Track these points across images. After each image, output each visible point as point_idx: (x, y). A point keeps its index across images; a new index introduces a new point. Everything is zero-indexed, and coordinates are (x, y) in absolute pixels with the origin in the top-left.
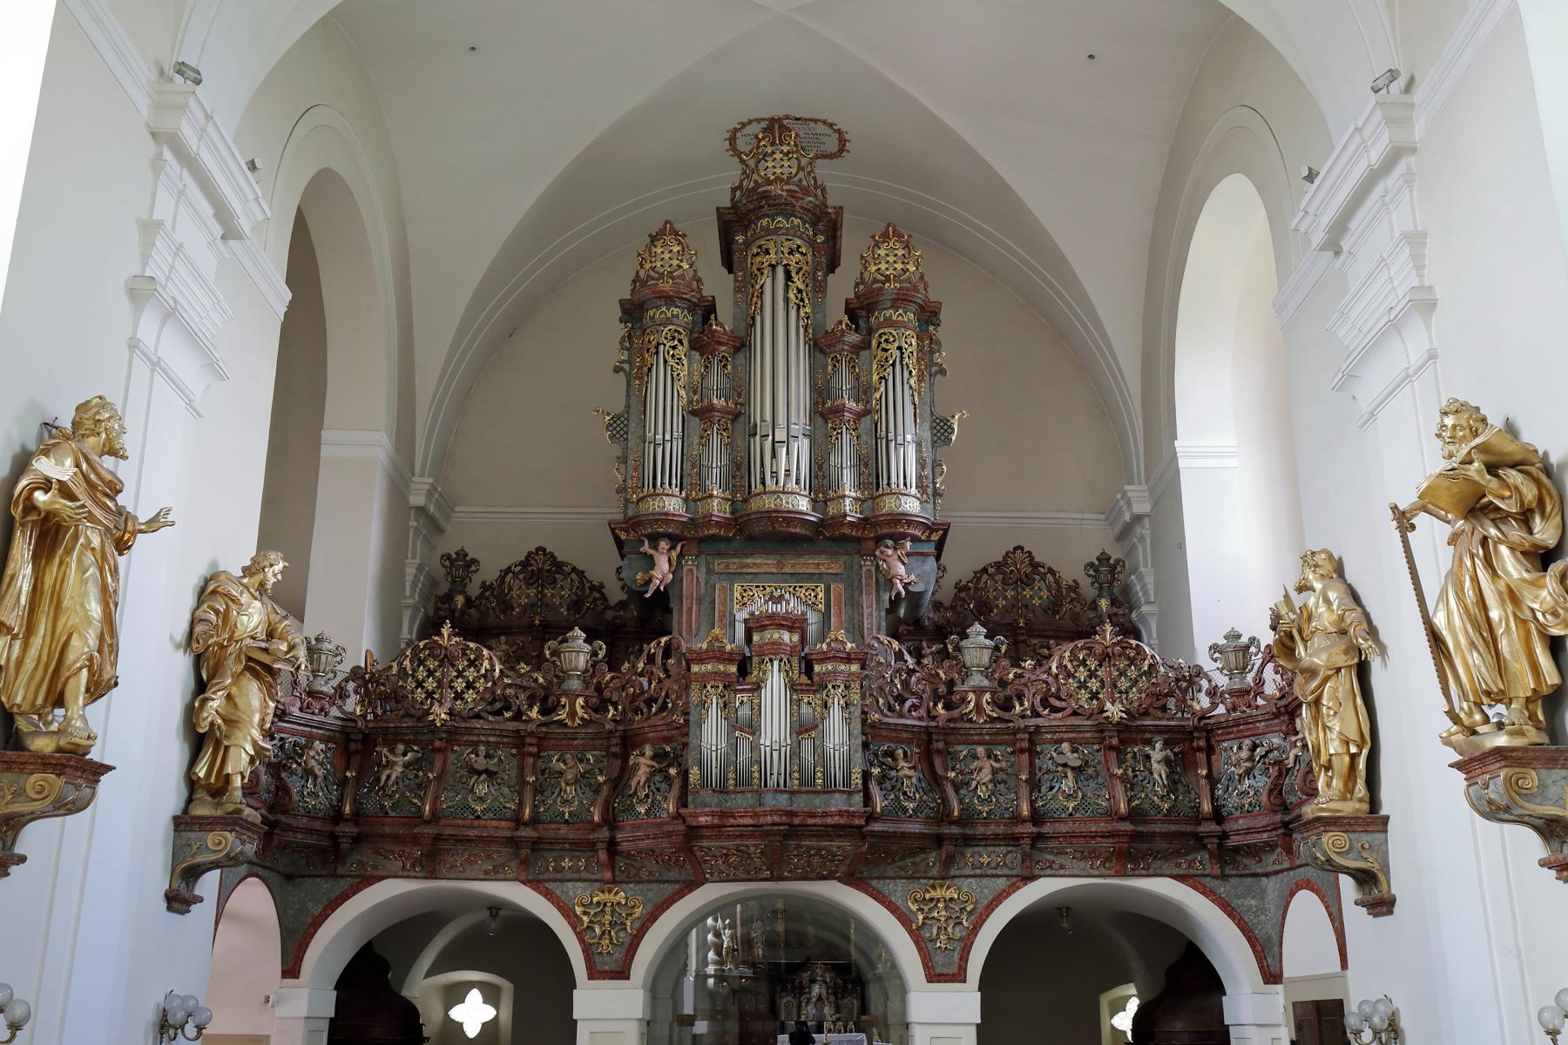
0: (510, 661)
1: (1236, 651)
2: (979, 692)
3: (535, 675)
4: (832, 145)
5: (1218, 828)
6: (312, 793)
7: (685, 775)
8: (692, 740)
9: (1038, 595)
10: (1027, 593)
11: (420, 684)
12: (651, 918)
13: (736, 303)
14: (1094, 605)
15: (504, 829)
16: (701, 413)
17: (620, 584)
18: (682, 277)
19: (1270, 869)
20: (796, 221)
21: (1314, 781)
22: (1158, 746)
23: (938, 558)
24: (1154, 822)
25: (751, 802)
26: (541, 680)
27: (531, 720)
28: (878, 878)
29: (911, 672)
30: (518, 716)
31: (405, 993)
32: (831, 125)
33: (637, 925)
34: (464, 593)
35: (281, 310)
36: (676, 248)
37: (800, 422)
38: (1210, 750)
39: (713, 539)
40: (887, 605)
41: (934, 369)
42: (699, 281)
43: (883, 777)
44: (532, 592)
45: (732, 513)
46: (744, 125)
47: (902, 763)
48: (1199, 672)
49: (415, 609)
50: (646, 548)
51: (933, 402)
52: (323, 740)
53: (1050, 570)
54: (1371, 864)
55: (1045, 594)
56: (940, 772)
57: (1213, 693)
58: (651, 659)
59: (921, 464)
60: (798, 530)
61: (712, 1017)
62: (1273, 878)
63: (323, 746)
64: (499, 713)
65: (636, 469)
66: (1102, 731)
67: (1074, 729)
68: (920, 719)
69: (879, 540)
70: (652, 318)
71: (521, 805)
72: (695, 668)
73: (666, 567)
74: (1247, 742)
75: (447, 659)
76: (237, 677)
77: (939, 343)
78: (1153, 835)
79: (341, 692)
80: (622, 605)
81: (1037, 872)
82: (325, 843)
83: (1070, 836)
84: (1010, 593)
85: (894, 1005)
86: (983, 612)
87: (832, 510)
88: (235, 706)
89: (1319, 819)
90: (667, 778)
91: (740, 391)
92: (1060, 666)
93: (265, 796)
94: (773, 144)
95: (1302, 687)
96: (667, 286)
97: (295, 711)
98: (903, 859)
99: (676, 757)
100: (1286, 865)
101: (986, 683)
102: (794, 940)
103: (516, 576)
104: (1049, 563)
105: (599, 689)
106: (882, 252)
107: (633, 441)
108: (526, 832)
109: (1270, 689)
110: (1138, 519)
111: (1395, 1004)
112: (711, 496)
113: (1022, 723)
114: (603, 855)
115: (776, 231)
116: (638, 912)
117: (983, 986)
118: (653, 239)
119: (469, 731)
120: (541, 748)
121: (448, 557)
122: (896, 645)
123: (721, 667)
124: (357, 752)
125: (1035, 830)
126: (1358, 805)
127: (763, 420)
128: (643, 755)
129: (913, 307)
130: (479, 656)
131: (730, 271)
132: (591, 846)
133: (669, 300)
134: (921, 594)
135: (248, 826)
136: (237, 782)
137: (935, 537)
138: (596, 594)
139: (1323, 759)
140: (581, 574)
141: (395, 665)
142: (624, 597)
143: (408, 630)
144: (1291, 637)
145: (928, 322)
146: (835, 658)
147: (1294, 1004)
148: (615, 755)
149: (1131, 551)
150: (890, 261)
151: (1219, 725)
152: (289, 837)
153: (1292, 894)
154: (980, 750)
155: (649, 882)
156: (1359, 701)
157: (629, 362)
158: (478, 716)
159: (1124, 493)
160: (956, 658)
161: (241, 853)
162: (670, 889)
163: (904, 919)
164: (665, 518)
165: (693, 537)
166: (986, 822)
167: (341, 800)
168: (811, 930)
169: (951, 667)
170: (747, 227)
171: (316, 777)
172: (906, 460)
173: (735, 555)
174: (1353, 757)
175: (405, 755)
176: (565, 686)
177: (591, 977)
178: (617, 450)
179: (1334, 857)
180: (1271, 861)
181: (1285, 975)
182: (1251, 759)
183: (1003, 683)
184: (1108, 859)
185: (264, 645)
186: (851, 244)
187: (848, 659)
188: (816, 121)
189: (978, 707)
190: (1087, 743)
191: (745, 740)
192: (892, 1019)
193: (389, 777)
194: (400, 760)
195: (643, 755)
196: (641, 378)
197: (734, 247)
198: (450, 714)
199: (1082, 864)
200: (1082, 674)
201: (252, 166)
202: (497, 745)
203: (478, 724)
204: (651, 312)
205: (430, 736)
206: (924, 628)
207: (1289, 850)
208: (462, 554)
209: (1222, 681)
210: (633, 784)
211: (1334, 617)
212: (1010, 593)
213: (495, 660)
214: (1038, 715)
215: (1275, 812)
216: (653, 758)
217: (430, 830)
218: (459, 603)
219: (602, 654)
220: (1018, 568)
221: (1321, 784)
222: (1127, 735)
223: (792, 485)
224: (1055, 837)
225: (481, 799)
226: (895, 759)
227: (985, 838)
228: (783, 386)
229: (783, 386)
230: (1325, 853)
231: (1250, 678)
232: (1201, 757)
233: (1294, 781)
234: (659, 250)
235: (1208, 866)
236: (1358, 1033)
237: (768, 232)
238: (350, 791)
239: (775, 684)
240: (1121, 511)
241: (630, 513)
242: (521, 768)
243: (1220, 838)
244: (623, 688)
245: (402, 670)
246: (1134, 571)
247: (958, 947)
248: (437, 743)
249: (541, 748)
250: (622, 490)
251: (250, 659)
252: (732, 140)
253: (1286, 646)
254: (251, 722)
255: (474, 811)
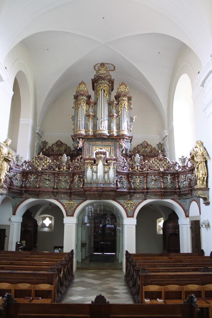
0: (53, 161)
1: (183, 160)
2: (138, 166)
3: (57, 162)
4: (113, 69)
5: (179, 191)
6: (17, 183)
7: (84, 181)
8: (85, 174)
9: (148, 150)
10: (146, 149)
11: (36, 164)
12: (78, 206)
13: (95, 96)
14: (158, 152)
15: (51, 190)
16: (88, 116)
17: (73, 147)
18: (85, 91)
19: (188, 198)
20: (106, 81)
21: (197, 181)
22: (169, 176)
23: (131, 143)
24: (168, 189)
25: (96, 185)
26: (58, 163)
27: (56, 171)
28: (119, 199)
29: (125, 163)
30: (54, 170)
31: (35, 218)
32: (112, 65)
33: (75, 207)
34: (45, 148)
35: (12, 95)
36: (84, 86)
37: (106, 118)
38: (178, 177)
39: (90, 138)
40: (121, 151)
41: (130, 108)
42: (88, 92)
43: (120, 181)
44: (57, 148)
45: (94, 134)
46: (97, 64)
47: (123, 179)
48: (177, 163)
49: (37, 151)
50: (78, 140)
51: (130, 115)
52: (19, 173)
53: (151, 146)
54: (206, 196)
55: (149, 149)
56: (130, 180)
57: (179, 167)
58: (78, 160)
59: (128, 126)
60: (105, 137)
61: (90, 223)
62: (188, 199)
63: (19, 175)
64: (50, 169)
65: (76, 126)
66: (159, 173)
67: (154, 173)
68: (127, 171)
69: (120, 139)
70: (79, 99)
71: (54, 186)
72: (86, 161)
73: (81, 143)
74: (185, 175)
75: (41, 159)
76: (2, 161)
77: (131, 104)
78: (167, 192)
79: (22, 165)
80: (74, 151)
81: (147, 198)
82: (20, 192)
83: (153, 192)
84: (143, 149)
85: (121, 221)
86: (138, 152)
87: (111, 134)
88: (2, 166)
89: (198, 188)
90: (81, 181)
91: (95, 112)
92: (152, 162)
93: (8, 183)
94: (102, 67)
95: (196, 165)
96: (82, 93)
97: (14, 168)
98: (123, 196)
99: (82, 177)
100: (191, 197)
101: (139, 165)
102: (105, 210)
103: (55, 145)
104: (150, 144)
105: (69, 165)
106: (121, 87)
107: (76, 121)
108: (55, 190)
109: (189, 166)
110: (166, 136)
111: (209, 221)
112: (90, 131)
113: (145, 172)
114: (69, 195)
115: (102, 83)
116: (75, 205)
117: (137, 218)
118: (80, 84)
119: (45, 172)
120: (58, 176)
121: (43, 142)
122: (123, 158)
123: (91, 161)
124: (25, 176)
125: (147, 191)
126: (204, 186)
127: (99, 117)
128: (76, 177)
129: (127, 97)
130: (47, 159)
131: (94, 91)
132: (67, 193)
133: (83, 95)
134: (127, 149)
135: (5, 188)
136: (3, 180)
137: (130, 139)
138: (69, 149)
139: (198, 178)
140: (66, 145)
141: (32, 160)
142: (74, 149)
143: (35, 155)
144: (194, 156)
145: (130, 100)
146: (111, 160)
147: (191, 221)
148: (71, 177)
149: (165, 142)
150: (123, 89)
151: (180, 172)
152: (13, 190)
153: (191, 202)
154: (137, 177)
155: (77, 200)
156: (205, 167)
157: (75, 106)
158: (47, 170)
159: (164, 132)
160: (134, 160)
161: (4, 193)
162: (81, 201)
163: (123, 206)
164: (81, 134)
165: (86, 138)
166: (138, 189)
167: (22, 184)
168: (107, 209)
169: (133, 162)
170: (97, 82)
171: (18, 180)
172: (125, 125)
173: (94, 142)
174: (204, 178)
175: (34, 176)
176: (62, 164)
177: (67, 216)
178: (73, 122)
179: (200, 195)
180: (189, 196)
181: (190, 216)
182: (185, 178)
183: (142, 165)
184: (160, 196)
185: (7, 156)
186: (116, 86)
187: (114, 160)
188: (109, 64)
189: (137, 169)
190: (157, 175)
191: (95, 175)
192: (121, 224)
193: (31, 180)
194: (33, 177)
195: (76, 177)
196: (77, 109)
197: (95, 86)
198: (42, 169)
199: (155, 197)
200: (156, 163)
201: (6, 68)
202: (50, 175)
203: (47, 171)
204: (79, 97)
205: (38, 173)
206: (129, 155)
207: (191, 195)
208: (45, 141)
209: (181, 165)
210: (75, 182)
211: (201, 152)
212: (143, 149)
213: (50, 159)
214: (148, 170)
215: (189, 188)
216: (79, 177)
217: (38, 190)
218: (44, 150)
219: (69, 159)
220: (145, 145)
221: (198, 183)
222: (163, 175)
223: (104, 129)
224: (150, 192)
225: (47, 184)
226: (122, 178)
227: (138, 192)
228: (103, 111)
229: (103, 111)
230: (198, 195)
231: (186, 164)
232: (177, 178)
233: (193, 182)
234: (81, 86)
235: (177, 197)
236: (202, 226)
237: (101, 83)
238: (24, 183)
239: (100, 164)
240: (163, 135)
241: (75, 134)
242: (54, 179)
243: (179, 192)
244: (73, 165)
245: (33, 161)
246: (165, 146)
247: (133, 211)
248: (39, 174)
249: (58, 176)
250: (73, 130)
251: (5, 158)
252: (95, 67)
253: (193, 158)
254: (5, 170)
255: (46, 187)
